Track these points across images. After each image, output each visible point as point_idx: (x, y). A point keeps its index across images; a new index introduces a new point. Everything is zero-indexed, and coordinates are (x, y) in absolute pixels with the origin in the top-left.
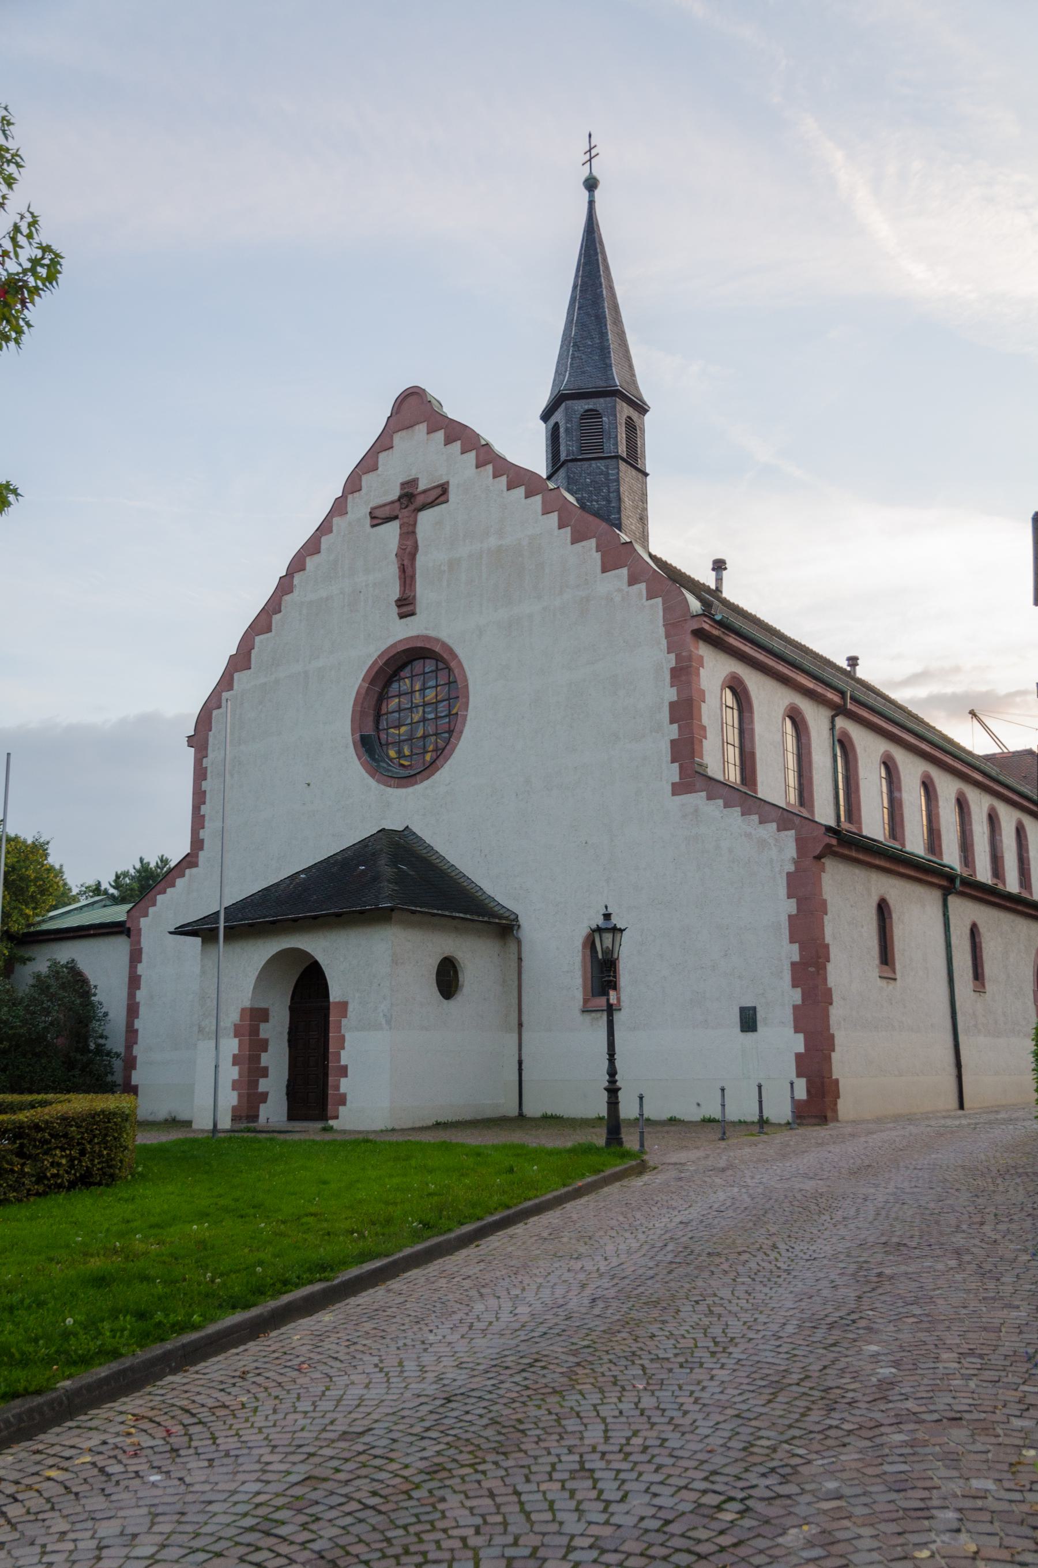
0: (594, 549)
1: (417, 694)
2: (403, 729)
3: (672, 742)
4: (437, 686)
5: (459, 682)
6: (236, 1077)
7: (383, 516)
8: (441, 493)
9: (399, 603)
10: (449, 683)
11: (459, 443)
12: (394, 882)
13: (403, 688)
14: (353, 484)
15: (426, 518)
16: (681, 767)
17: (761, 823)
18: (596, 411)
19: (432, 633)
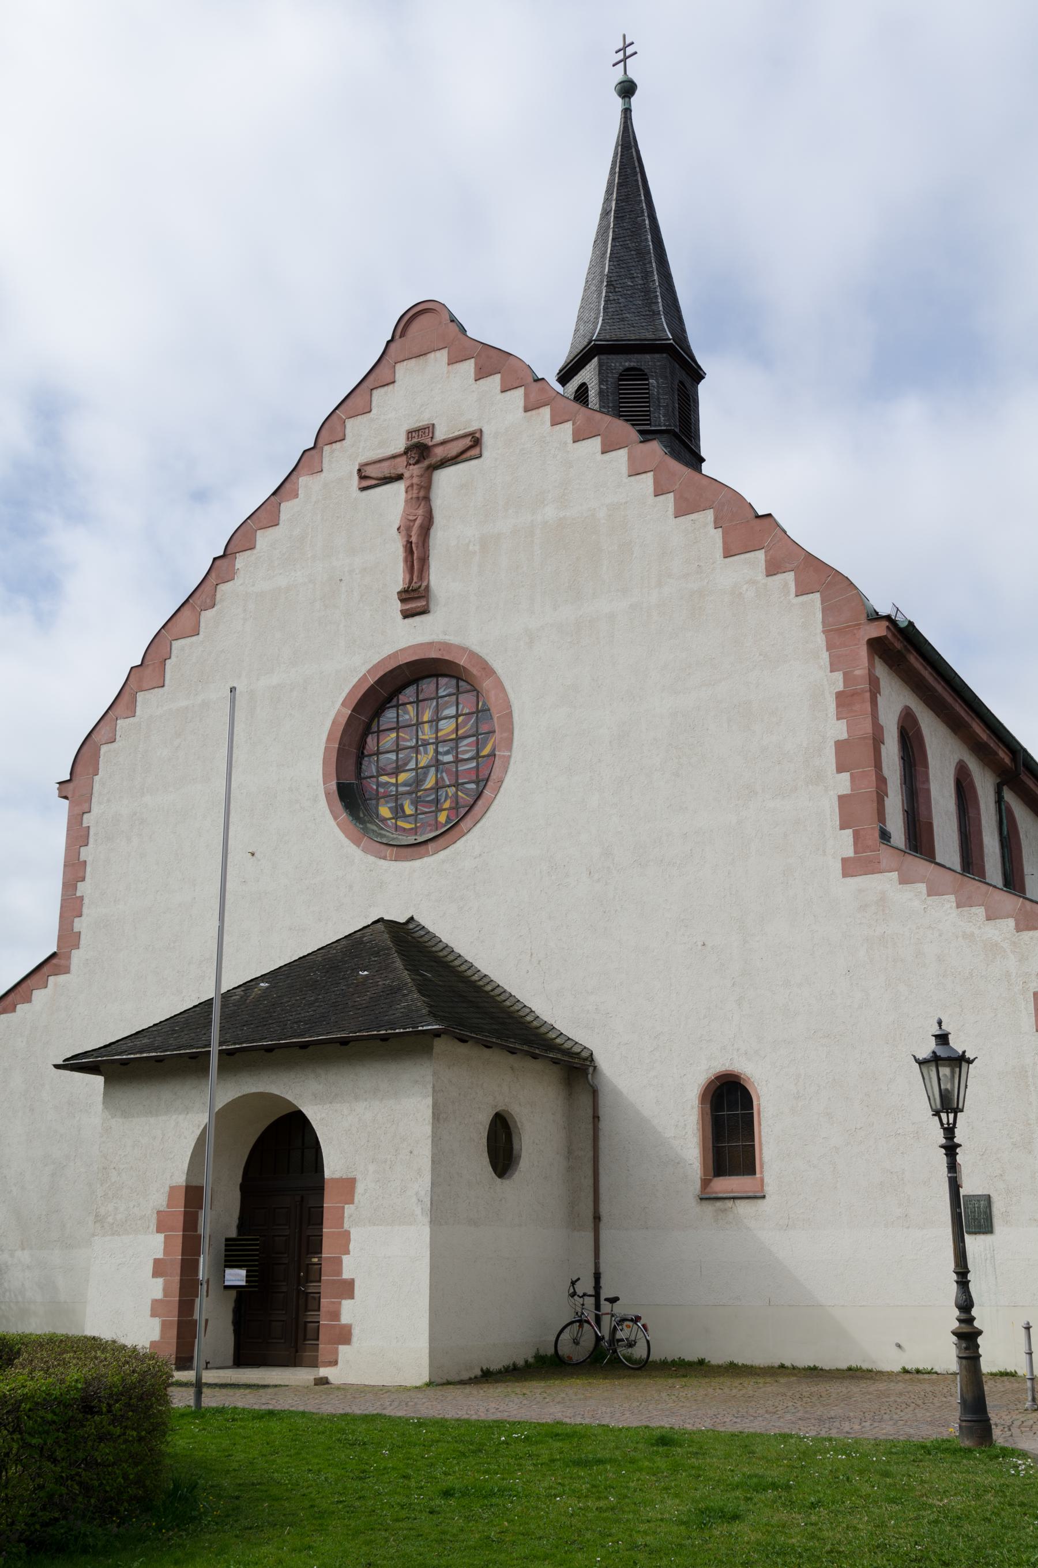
0: (712, 525)
1: (426, 726)
2: (403, 777)
3: (841, 798)
4: (457, 716)
5: (493, 710)
6: (159, 1295)
7: (380, 475)
8: (472, 445)
9: (404, 596)
10: (478, 711)
11: (498, 377)
12: (399, 997)
13: (404, 718)
14: (331, 430)
15: (446, 479)
16: (856, 836)
17: (988, 918)
18: (641, 370)
19: (453, 639)
